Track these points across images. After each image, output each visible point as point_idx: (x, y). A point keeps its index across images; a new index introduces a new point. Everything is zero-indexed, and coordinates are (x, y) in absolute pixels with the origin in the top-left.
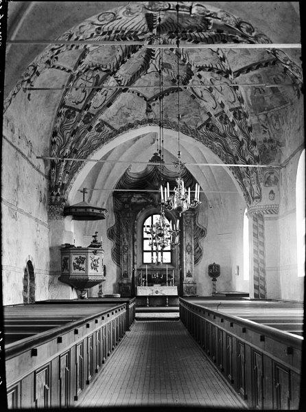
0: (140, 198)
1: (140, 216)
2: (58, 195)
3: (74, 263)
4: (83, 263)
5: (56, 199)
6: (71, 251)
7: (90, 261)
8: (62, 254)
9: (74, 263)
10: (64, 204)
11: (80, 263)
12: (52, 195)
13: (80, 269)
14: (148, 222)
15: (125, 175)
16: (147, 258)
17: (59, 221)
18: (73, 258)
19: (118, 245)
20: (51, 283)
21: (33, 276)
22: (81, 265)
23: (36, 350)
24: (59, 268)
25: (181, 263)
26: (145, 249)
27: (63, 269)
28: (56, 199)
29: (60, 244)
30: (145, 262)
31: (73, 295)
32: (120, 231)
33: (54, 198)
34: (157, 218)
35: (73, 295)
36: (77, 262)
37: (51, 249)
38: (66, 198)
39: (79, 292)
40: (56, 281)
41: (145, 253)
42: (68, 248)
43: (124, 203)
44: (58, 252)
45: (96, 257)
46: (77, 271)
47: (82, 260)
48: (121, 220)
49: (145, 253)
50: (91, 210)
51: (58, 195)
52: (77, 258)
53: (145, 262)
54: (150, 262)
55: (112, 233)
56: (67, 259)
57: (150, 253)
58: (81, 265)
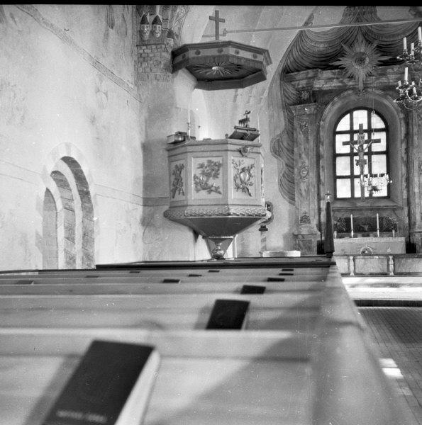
0: (330, 79)
1: (330, 111)
2: (156, 21)
3: (195, 177)
4: (216, 176)
5: (152, 33)
6: (189, 149)
7: (232, 172)
8: (171, 158)
9: (195, 177)
10: (171, 42)
11: (208, 175)
12: (144, 21)
13: (210, 190)
14: (344, 125)
15: (301, 36)
16: (343, 190)
17: (161, 83)
18: (194, 166)
19: (290, 166)
20: (147, 222)
21: (90, 201)
22: (212, 182)
23: (318, 254)
24: (164, 190)
25: (408, 195)
26: (339, 173)
27: (174, 192)
28: (152, 33)
29: (165, 138)
30: (339, 196)
31: (201, 252)
32: (293, 141)
33: (147, 29)
34: (360, 117)
35: (201, 252)
36: (203, 173)
37: (146, 148)
38: (175, 30)
39: (212, 243)
40: (159, 216)
41: (339, 181)
42: (180, 143)
43: (299, 91)
44: (161, 155)
45: (246, 162)
46: (203, 193)
47: (214, 170)
48: (296, 123)
49: (339, 181)
50: (231, 51)
51: (156, 21)
52: (202, 166)
53: (339, 196)
54: (348, 195)
55: (279, 146)
56: (180, 169)
57: (348, 181)
58: (212, 182)
